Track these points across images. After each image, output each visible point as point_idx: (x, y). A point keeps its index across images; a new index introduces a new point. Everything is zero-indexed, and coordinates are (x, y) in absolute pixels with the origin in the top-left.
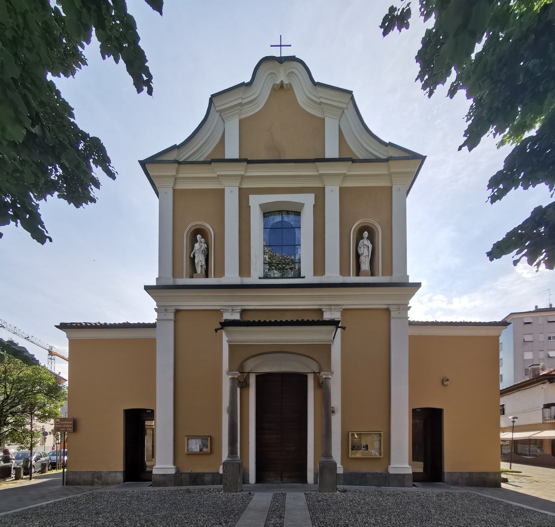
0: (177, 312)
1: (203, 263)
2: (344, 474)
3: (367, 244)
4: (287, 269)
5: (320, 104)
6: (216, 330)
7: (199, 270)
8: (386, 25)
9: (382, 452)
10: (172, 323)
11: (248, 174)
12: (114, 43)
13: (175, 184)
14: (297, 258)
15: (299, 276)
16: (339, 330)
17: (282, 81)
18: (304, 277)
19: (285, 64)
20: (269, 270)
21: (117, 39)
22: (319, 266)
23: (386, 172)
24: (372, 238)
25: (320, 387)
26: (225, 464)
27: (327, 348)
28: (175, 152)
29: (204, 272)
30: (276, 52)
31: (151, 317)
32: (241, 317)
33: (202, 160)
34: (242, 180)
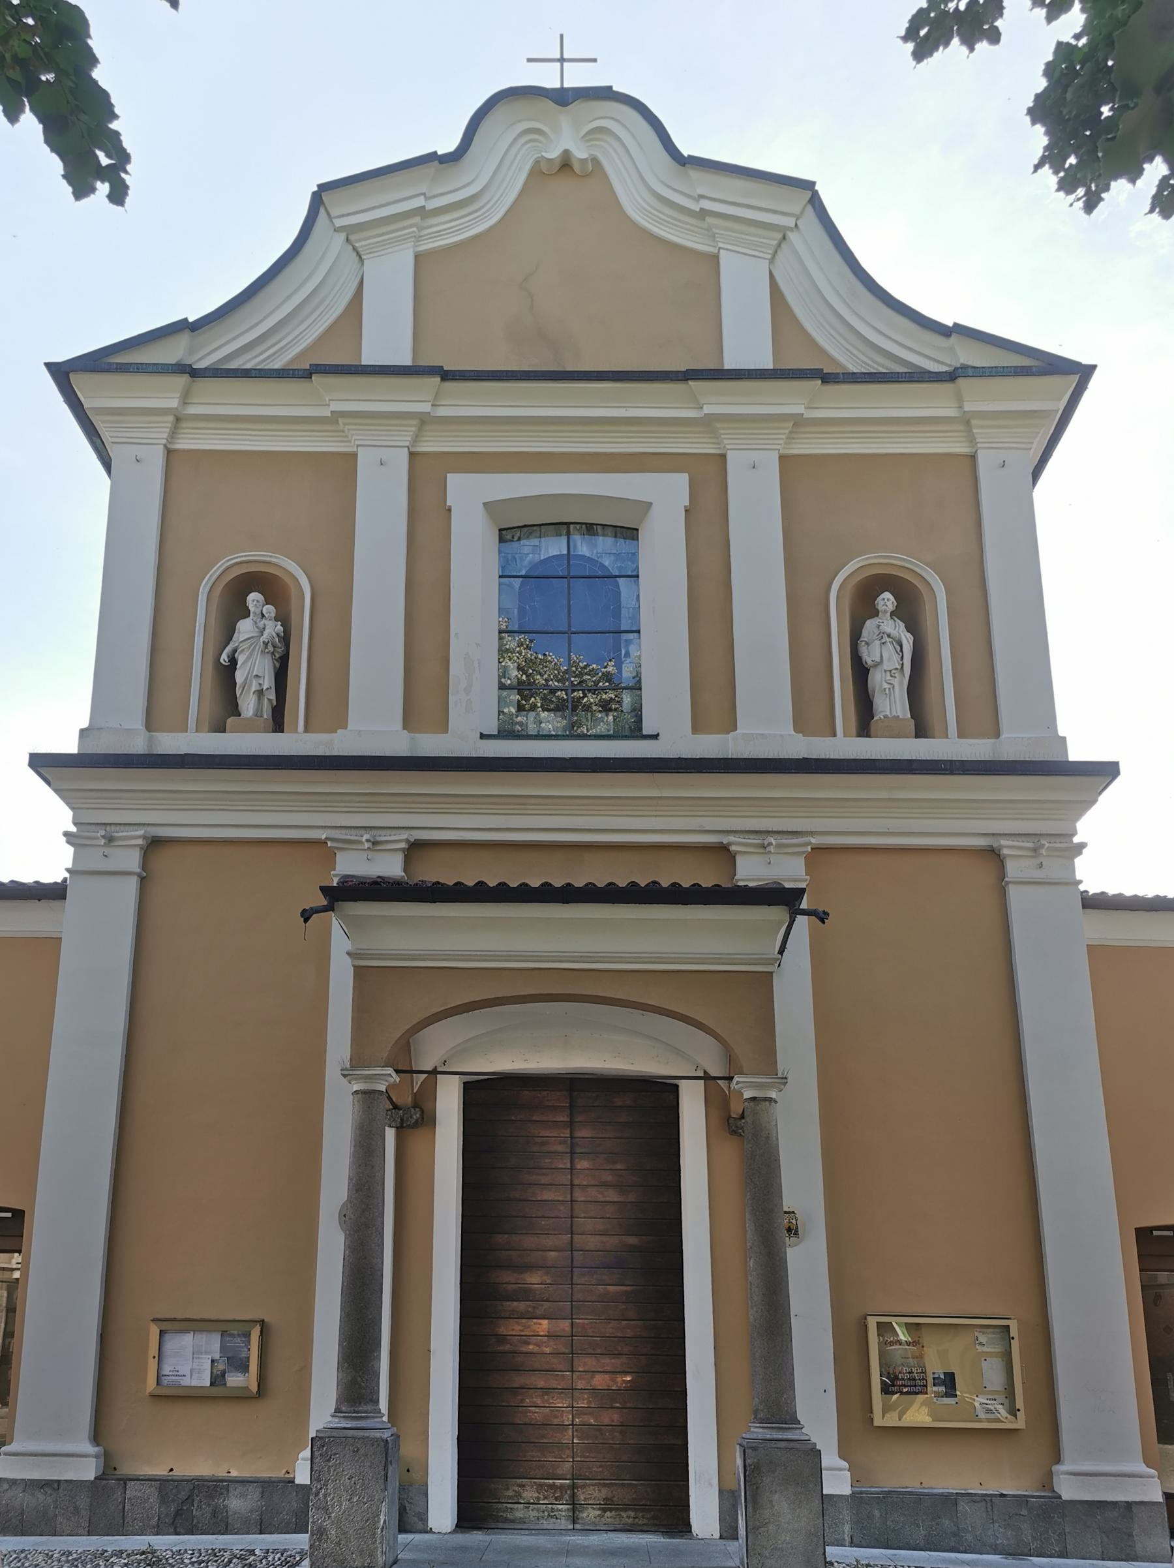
0: (154, 845)
1: (268, 682)
2: (856, 1498)
3: (894, 633)
4: (588, 708)
5: (703, 214)
6: (306, 915)
7: (248, 705)
8: (923, 33)
9: (1020, 1404)
10: (133, 883)
11: (442, 412)
12: (10, 73)
13: (174, 433)
14: (627, 672)
15: (636, 732)
16: (801, 920)
17: (566, 153)
18: (655, 737)
19: (577, 107)
20: (520, 708)
21: (21, 63)
22: (714, 697)
23: (951, 413)
24: (910, 610)
25: (734, 1132)
26: (322, 1445)
27: (756, 987)
28: (184, 339)
29: (267, 713)
30: (548, 78)
31: (50, 862)
32: (406, 869)
33: (277, 365)
34: (420, 429)
